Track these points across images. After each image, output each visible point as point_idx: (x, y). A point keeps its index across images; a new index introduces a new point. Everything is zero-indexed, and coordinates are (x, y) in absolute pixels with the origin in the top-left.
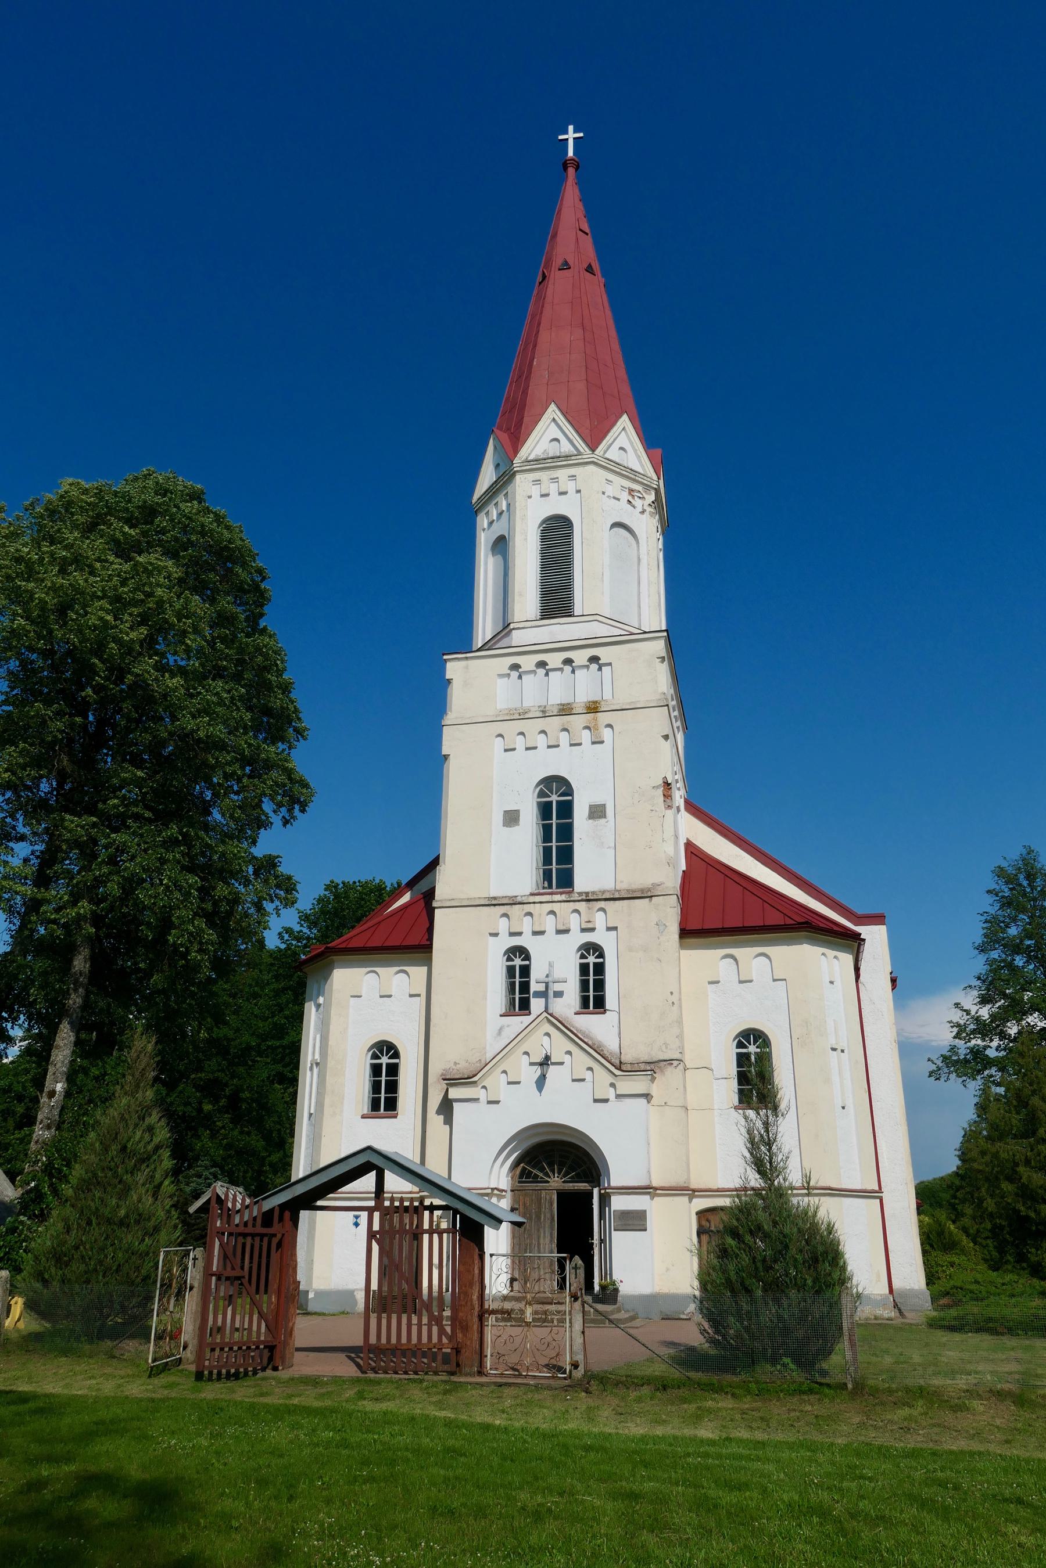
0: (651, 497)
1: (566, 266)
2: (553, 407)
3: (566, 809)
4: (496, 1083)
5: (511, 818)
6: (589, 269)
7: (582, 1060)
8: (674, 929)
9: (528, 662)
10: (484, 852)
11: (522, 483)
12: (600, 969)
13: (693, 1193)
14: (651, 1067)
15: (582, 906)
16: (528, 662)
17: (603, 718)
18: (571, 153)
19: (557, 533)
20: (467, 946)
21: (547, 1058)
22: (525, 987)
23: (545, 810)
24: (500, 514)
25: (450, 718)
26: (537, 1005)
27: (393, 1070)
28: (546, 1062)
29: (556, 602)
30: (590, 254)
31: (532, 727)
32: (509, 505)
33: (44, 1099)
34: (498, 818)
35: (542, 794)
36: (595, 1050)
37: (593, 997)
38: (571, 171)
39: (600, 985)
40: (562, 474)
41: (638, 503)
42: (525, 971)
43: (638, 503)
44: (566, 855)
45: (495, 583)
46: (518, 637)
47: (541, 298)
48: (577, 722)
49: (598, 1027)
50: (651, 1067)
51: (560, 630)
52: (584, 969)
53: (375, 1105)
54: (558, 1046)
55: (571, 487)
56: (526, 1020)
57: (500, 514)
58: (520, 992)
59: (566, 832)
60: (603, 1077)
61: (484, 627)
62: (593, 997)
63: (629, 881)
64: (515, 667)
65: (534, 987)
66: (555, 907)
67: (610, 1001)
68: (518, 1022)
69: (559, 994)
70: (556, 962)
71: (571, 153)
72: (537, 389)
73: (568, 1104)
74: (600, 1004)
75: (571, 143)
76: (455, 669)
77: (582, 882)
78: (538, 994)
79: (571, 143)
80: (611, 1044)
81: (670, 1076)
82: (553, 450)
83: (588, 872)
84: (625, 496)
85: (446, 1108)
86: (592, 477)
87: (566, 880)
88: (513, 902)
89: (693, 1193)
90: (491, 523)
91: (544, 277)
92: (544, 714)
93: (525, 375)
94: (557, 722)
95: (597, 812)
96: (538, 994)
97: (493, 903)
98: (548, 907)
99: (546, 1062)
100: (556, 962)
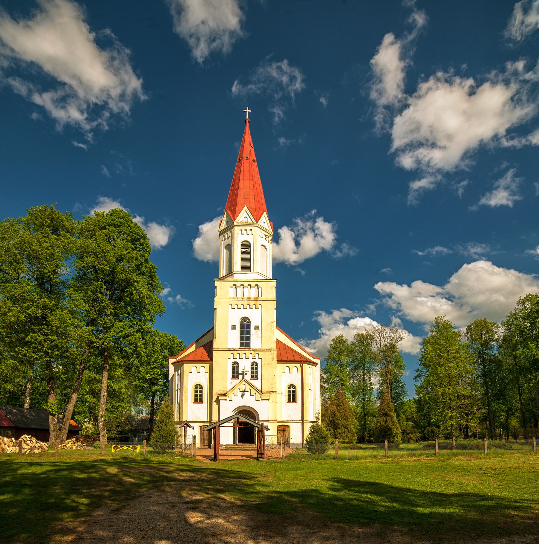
0: (271, 238)
1: (247, 159)
2: (246, 207)
3: (248, 326)
4: (231, 395)
5: (234, 327)
6: (254, 161)
7: (253, 391)
8: (276, 359)
9: (238, 284)
10: (226, 337)
11: (236, 229)
12: (257, 369)
13: (276, 421)
14: (269, 393)
15: (253, 352)
16: (238, 284)
17: (259, 302)
18: (247, 117)
19: (246, 246)
20: (222, 362)
21: (245, 390)
22: (237, 372)
23: (242, 326)
24: (228, 237)
25: (216, 298)
26: (241, 377)
27: (201, 392)
28: (244, 391)
29: (246, 267)
30: (254, 156)
31: (239, 303)
32: (232, 235)
33: (102, 397)
34: (230, 327)
35: (242, 322)
36: (255, 388)
37: (255, 376)
38: (247, 123)
39: (257, 372)
40: (248, 228)
41: (267, 239)
42: (238, 368)
43: (267, 239)
44: (248, 338)
45: (226, 258)
46: (236, 276)
47: (240, 168)
48: (252, 303)
49: (256, 383)
50: (269, 393)
51: (246, 276)
52: (252, 368)
53: (196, 400)
54: (248, 387)
55: (250, 232)
56: (238, 381)
57: (228, 237)
58: (235, 373)
59: (248, 332)
60: (258, 395)
61: (223, 271)
62: (255, 376)
63: (265, 347)
64: (235, 285)
65: (240, 372)
66: (246, 352)
67: (259, 377)
68: (236, 381)
69: (246, 374)
70: (245, 365)
71: (247, 117)
72: (240, 200)
73: (249, 401)
74: (257, 378)
75: (247, 113)
76: (217, 284)
77: (253, 346)
78: (241, 374)
79: (247, 113)
80: (259, 388)
81: (273, 395)
82: (245, 220)
83: (255, 343)
84: (264, 237)
85: (218, 401)
86: (256, 230)
87: (248, 345)
88: (235, 350)
89: (276, 421)
90: (225, 239)
91: (240, 160)
92: (243, 300)
93: (235, 192)
94: (246, 302)
95: (257, 328)
96: (241, 374)
97: (229, 350)
98: (244, 352)
99: (244, 391)
100: (245, 365)
